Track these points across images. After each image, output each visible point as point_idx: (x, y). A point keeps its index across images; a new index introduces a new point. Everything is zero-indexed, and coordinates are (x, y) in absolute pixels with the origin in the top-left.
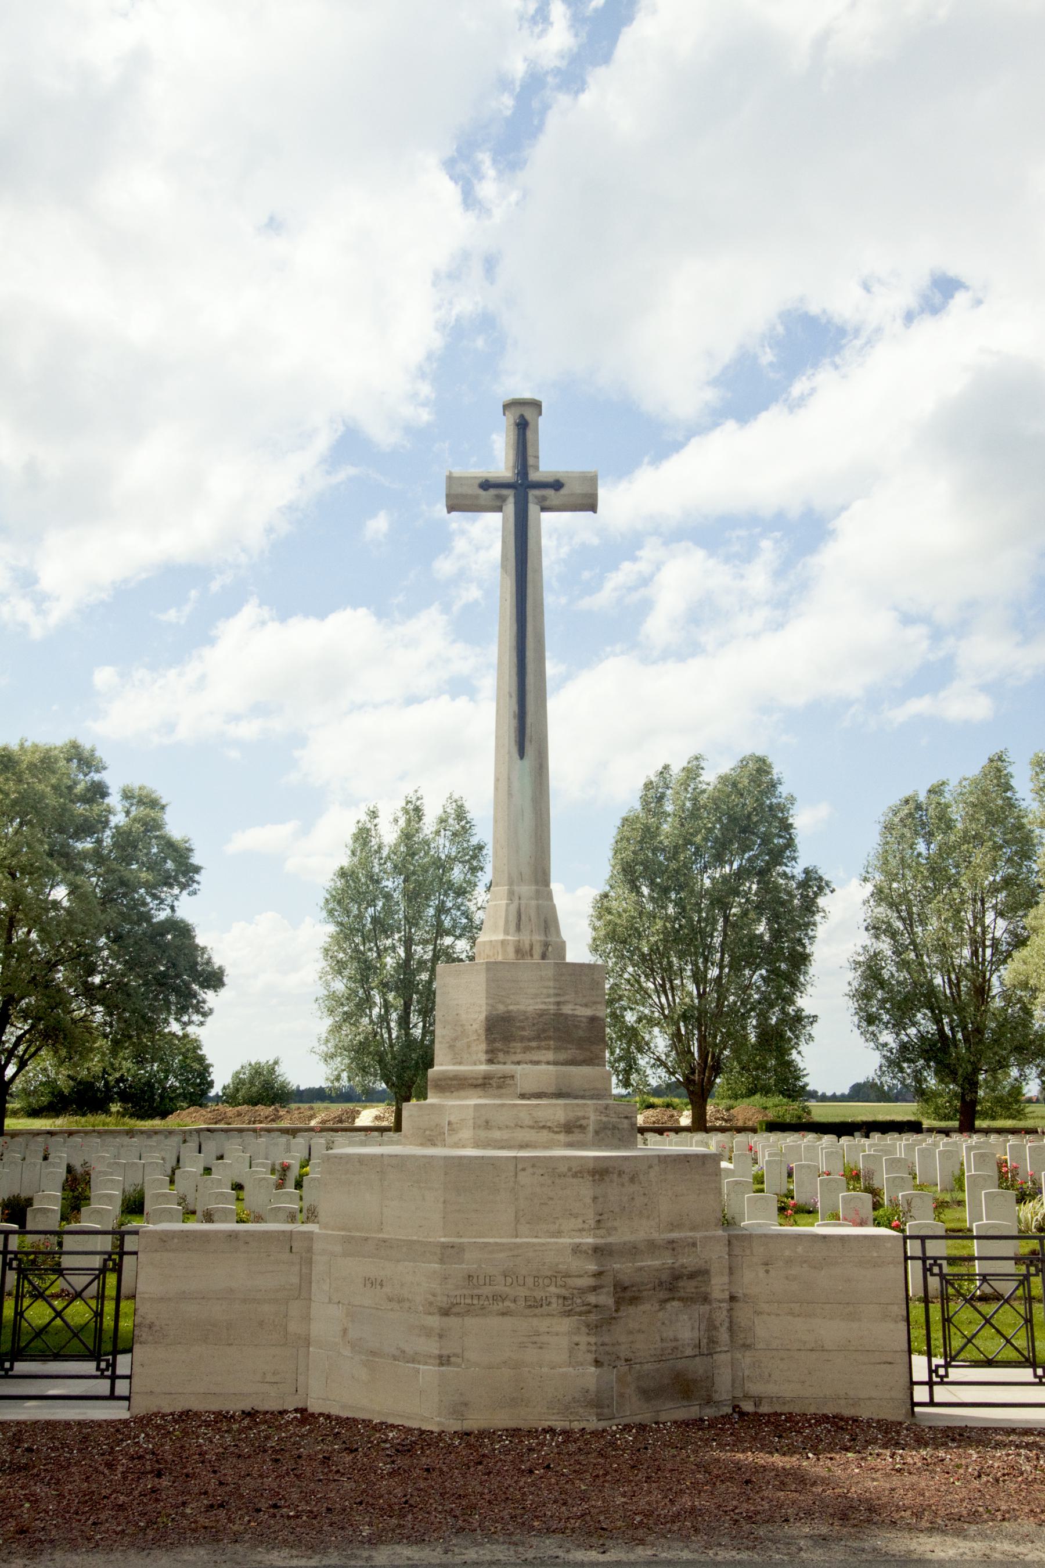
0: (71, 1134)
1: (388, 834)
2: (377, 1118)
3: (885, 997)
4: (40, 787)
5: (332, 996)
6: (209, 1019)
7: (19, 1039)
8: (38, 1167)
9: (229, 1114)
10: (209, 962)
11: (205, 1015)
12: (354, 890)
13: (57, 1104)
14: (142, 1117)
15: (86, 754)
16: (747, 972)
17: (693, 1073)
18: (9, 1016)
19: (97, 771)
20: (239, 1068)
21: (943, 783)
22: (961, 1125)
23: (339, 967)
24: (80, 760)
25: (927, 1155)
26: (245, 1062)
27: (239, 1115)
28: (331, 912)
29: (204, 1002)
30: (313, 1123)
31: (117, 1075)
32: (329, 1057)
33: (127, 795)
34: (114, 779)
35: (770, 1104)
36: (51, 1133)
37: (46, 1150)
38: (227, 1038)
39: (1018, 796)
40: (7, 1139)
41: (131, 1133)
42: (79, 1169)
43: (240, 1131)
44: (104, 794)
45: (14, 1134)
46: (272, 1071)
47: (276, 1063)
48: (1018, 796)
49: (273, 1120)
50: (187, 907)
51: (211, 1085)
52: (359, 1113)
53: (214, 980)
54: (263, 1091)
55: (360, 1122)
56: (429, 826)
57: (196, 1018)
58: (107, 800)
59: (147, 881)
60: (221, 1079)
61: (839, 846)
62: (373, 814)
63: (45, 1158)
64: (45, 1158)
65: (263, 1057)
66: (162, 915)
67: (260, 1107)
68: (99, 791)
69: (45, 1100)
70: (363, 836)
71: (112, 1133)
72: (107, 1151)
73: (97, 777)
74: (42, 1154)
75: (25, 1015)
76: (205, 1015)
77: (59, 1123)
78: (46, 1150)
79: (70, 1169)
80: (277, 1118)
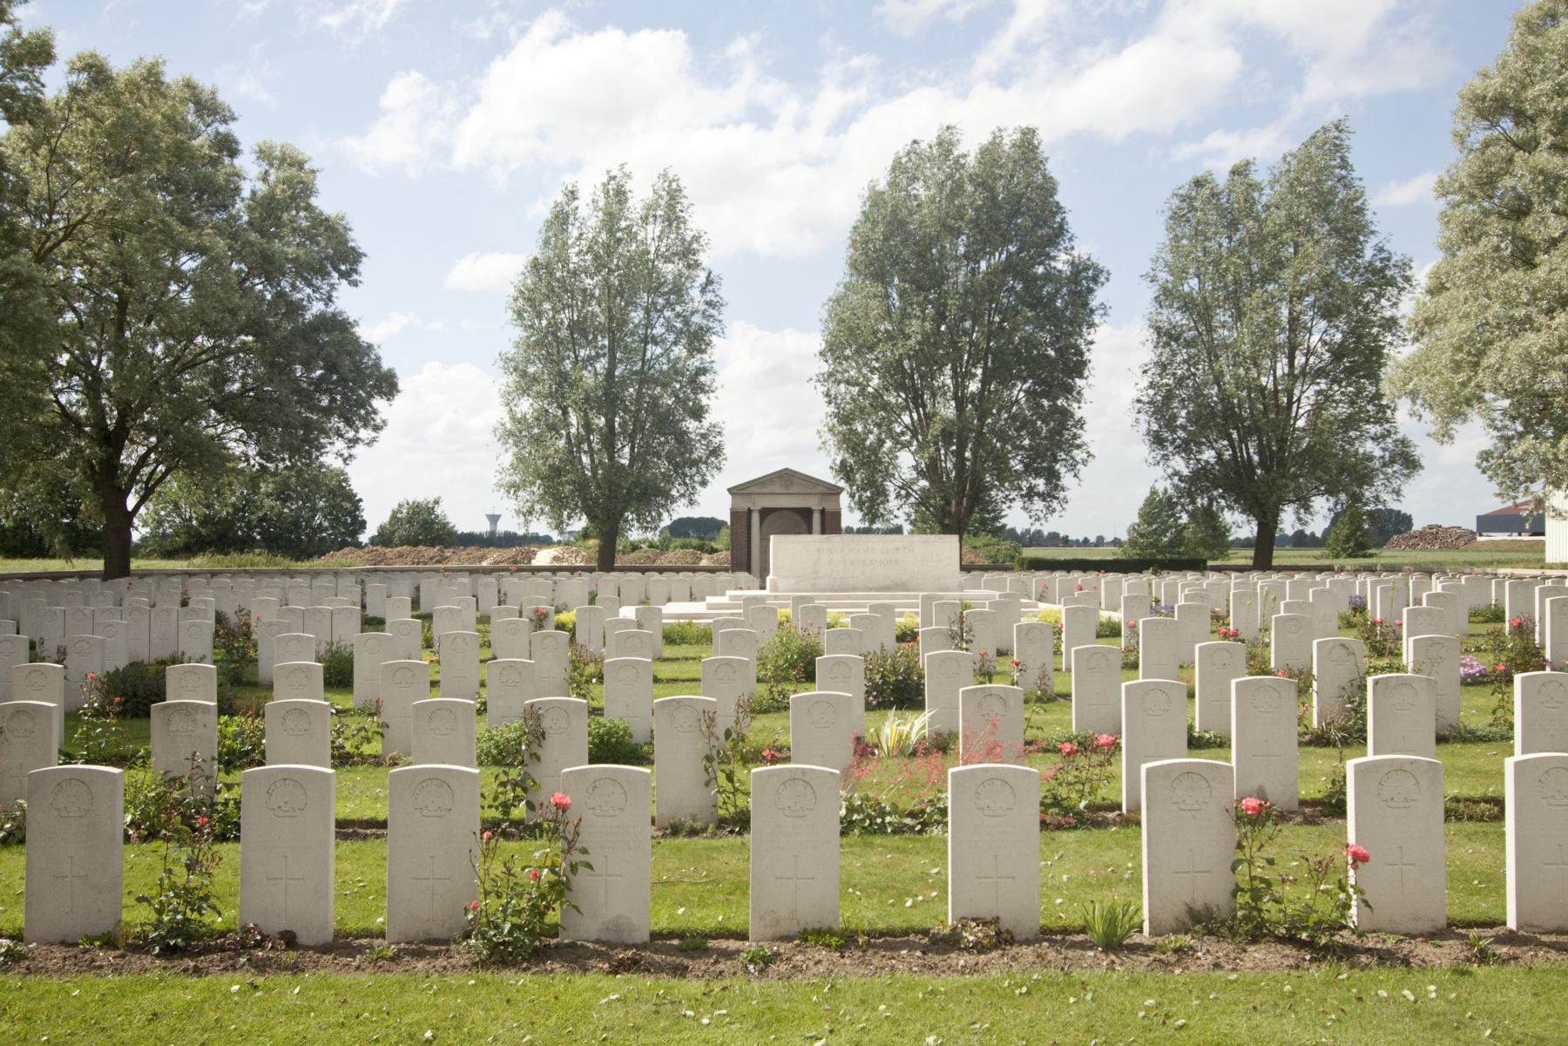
0: (214, 574)
1: (588, 216)
2: (555, 559)
3: (1174, 416)
4: (148, 113)
5: (520, 421)
6: (382, 434)
7: (143, 460)
8: (174, 617)
9: (389, 555)
10: (377, 365)
11: (377, 428)
12: (547, 284)
13: (192, 544)
14: (298, 560)
15: (205, 97)
16: (1006, 393)
17: (948, 503)
18: (128, 432)
19: (225, 122)
20: (395, 507)
21: (1248, 163)
22: (1256, 558)
23: (527, 383)
24: (197, 103)
25: (1246, 596)
26: (402, 500)
27: (401, 555)
28: (519, 314)
29: (375, 412)
30: (484, 564)
31: (260, 514)
32: (514, 487)
33: (264, 154)
34: (247, 134)
35: (978, 544)
36: (191, 574)
37: (185, 593)
38: (380, 472)
39: (1354, 175)
40: (135, 580)
41: (292, 574)
42: (233, 620)
43: (403, 571)
44: (233, 153)
45: (143, 574)
46: (430, 511)
47: (436, 502)
48: (1354, 175)
49: (439, 562)
50: (347, 300)
51: (363, 525)
52: (535, 553)
53: (387, 385)
54: (422, 530)
55: (535, 563)
56: (636, 204)
57: (365, 434)
58: (237, 162)
59: (298, 258)
60: (375, 517)
61: (1119, 242)
62: (572, 195)
63: (184, 604)
64: (184, 604)
65: (422, 495)
66: (317, 307)
67: (421, 548)
68: (228, 146)
69: (180, 541)
70: (561, 219)
71: (265, 573)
72: (271, 594)
73: (222, 129)
74: (179, 599)
75: (148, 429)
76: (377, 428)
77: (200, 562)
78: (185, 593)
79: (220, 619)
80: (482, 558)
